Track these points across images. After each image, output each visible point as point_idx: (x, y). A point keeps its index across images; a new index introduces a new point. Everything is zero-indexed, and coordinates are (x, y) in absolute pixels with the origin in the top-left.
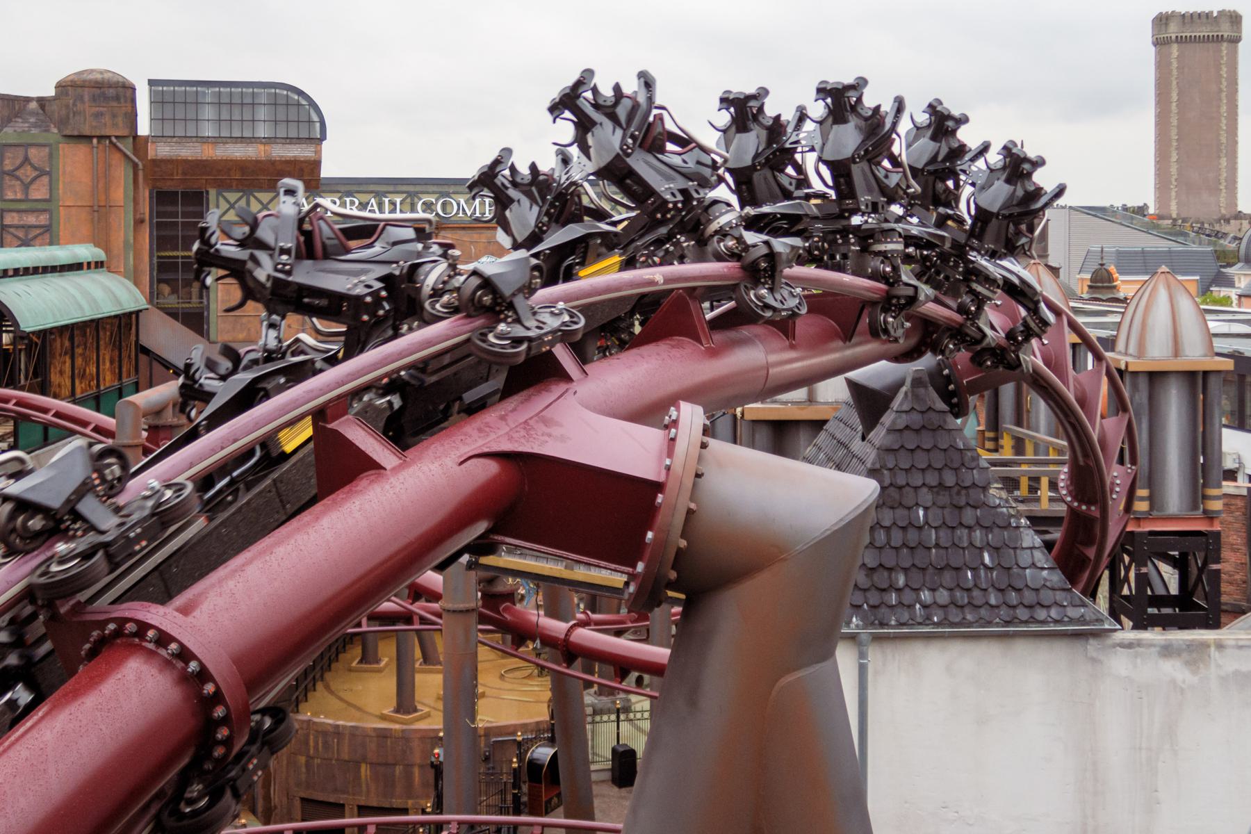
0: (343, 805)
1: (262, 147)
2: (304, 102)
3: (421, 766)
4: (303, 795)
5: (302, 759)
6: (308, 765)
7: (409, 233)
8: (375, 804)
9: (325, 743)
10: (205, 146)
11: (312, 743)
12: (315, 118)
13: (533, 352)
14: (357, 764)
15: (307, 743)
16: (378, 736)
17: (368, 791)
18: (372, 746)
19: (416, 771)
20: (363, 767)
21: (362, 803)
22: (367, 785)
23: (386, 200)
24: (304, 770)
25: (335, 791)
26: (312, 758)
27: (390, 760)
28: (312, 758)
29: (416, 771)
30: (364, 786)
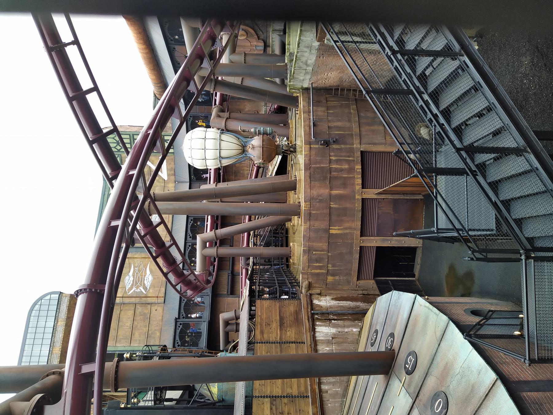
0: (361, 247)
1: (59, 323)
2: (39, 303)
3: (331, 189)
4: (355, 278)
5: (330, 279)
6: (333, 275)
7: (255, 238)
8: (359, 223)
9: (317, 261)
10: (54, 352)
11: (318, 271)
12: (48, 297)
13: (115, 153)
14: (330, 236)
15: (318, 274)
16: (310, 220)
17: (350, 228)
18: (317, 224)
19: (334, 192)
20: (332, 232)
21: (359, 233)
22: (346, 229)
23: (242, 350)
24: (337, 278)
25: (351, 253)
26: (328, 270)
27: (327, 211)
28: (328, 270)
29: (334, 192)
30: (348, 231)
